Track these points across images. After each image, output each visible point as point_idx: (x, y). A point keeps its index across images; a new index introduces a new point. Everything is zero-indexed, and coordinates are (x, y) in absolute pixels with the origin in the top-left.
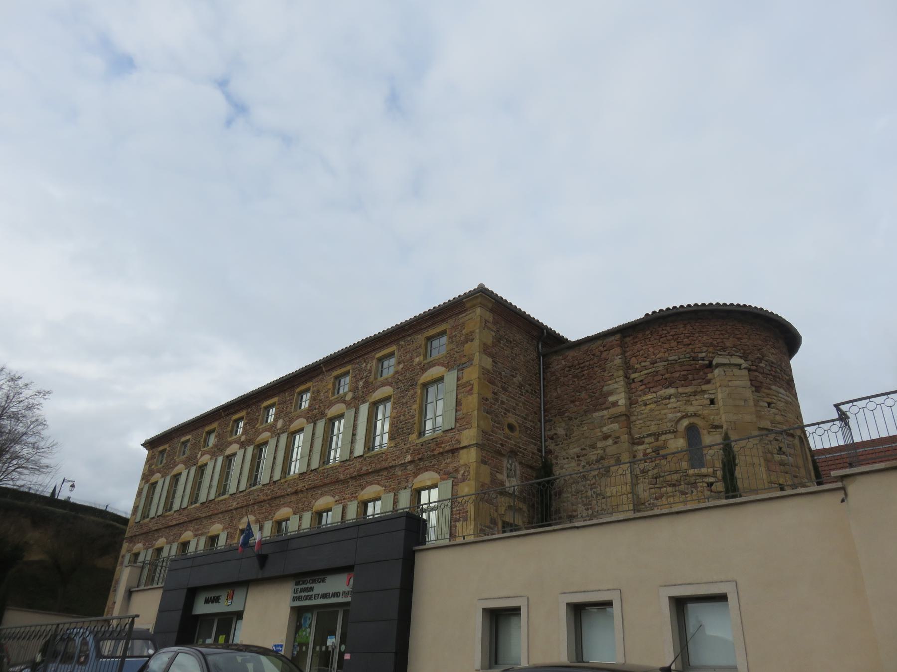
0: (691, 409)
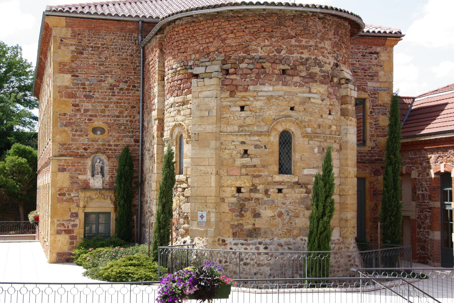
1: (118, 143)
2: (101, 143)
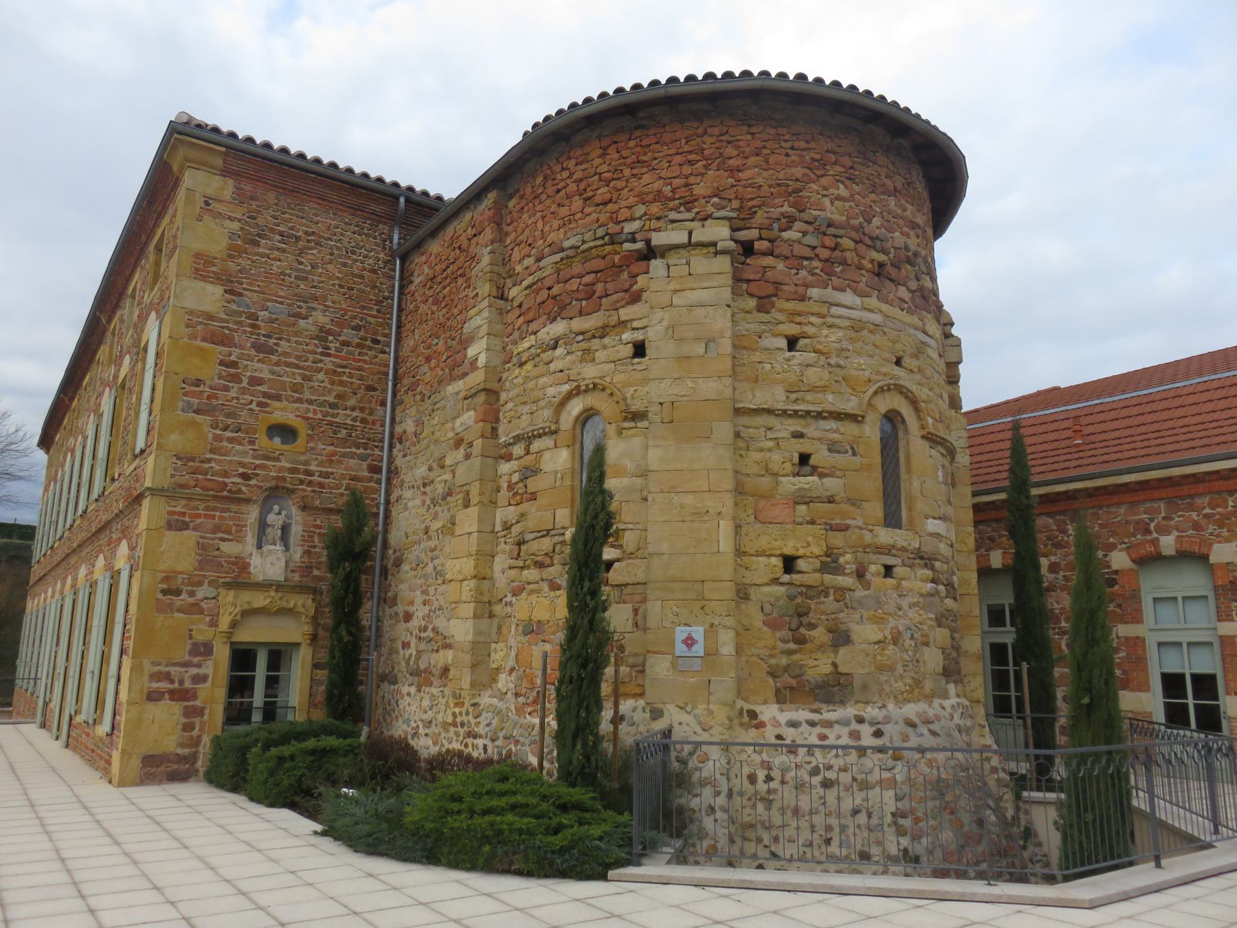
0: (590, 372)
1: (330, 470)
2: (288, 465)
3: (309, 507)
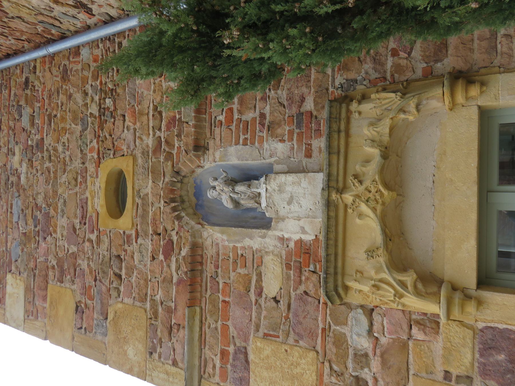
3: (196, 140)
